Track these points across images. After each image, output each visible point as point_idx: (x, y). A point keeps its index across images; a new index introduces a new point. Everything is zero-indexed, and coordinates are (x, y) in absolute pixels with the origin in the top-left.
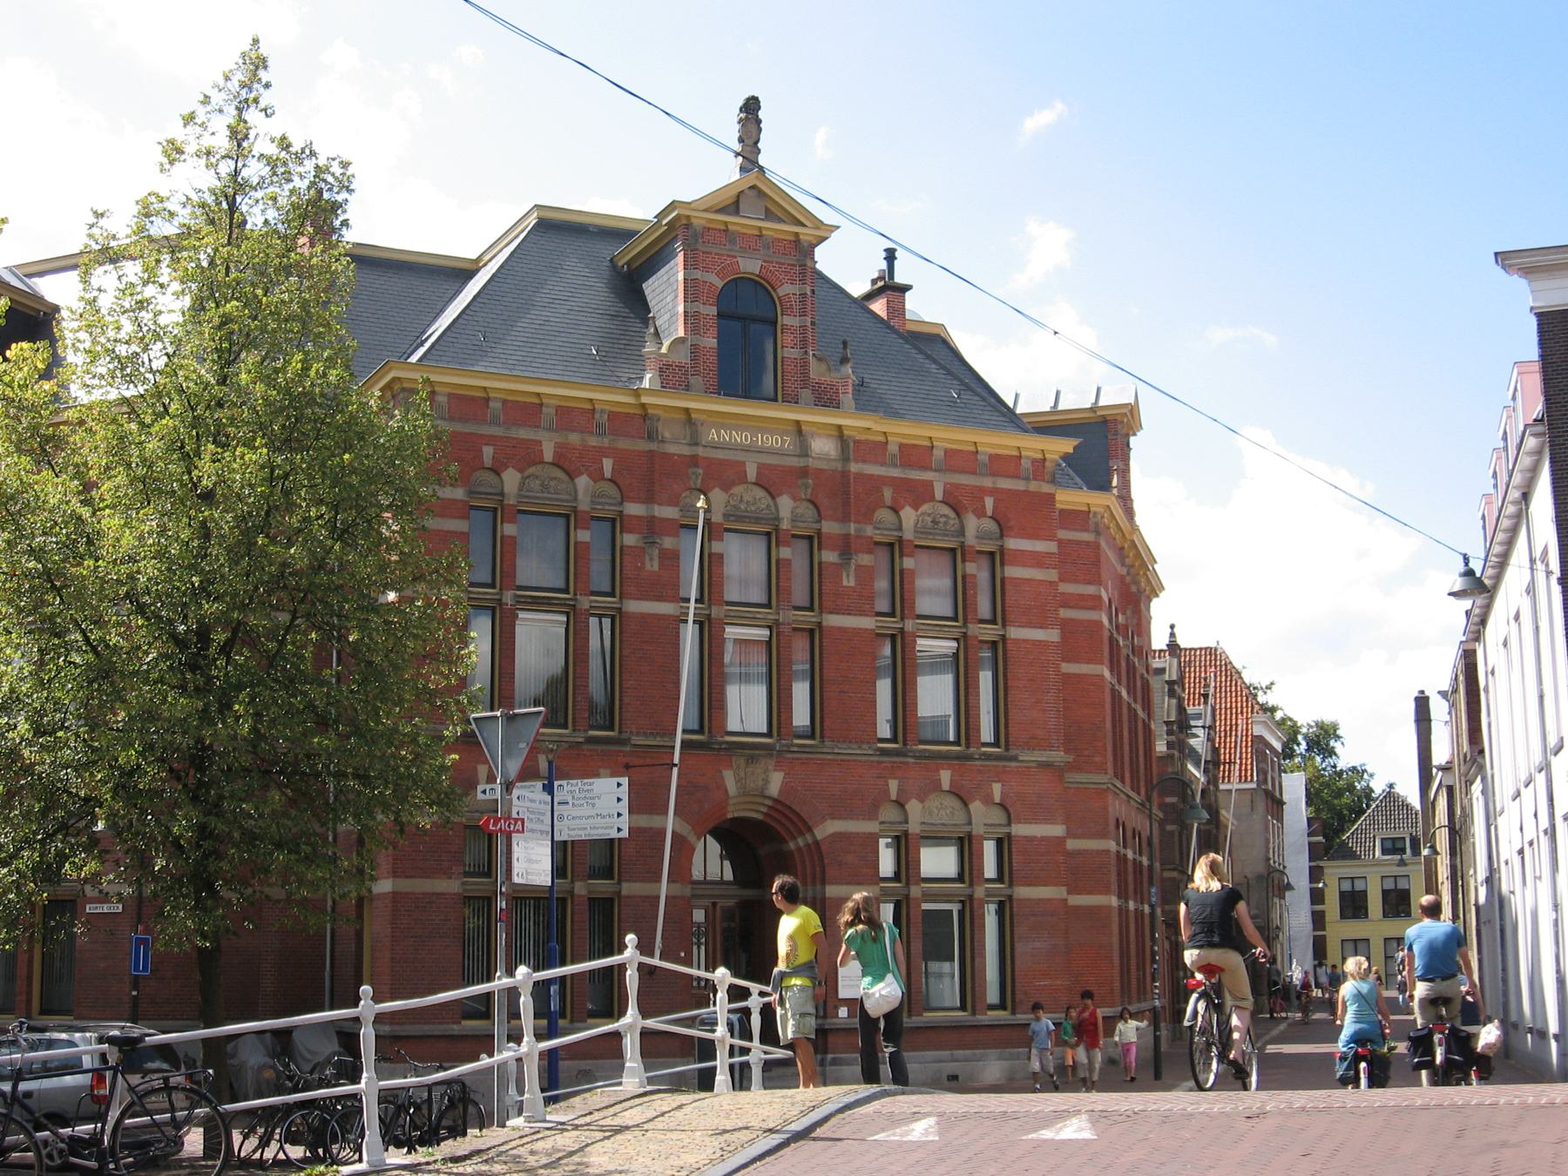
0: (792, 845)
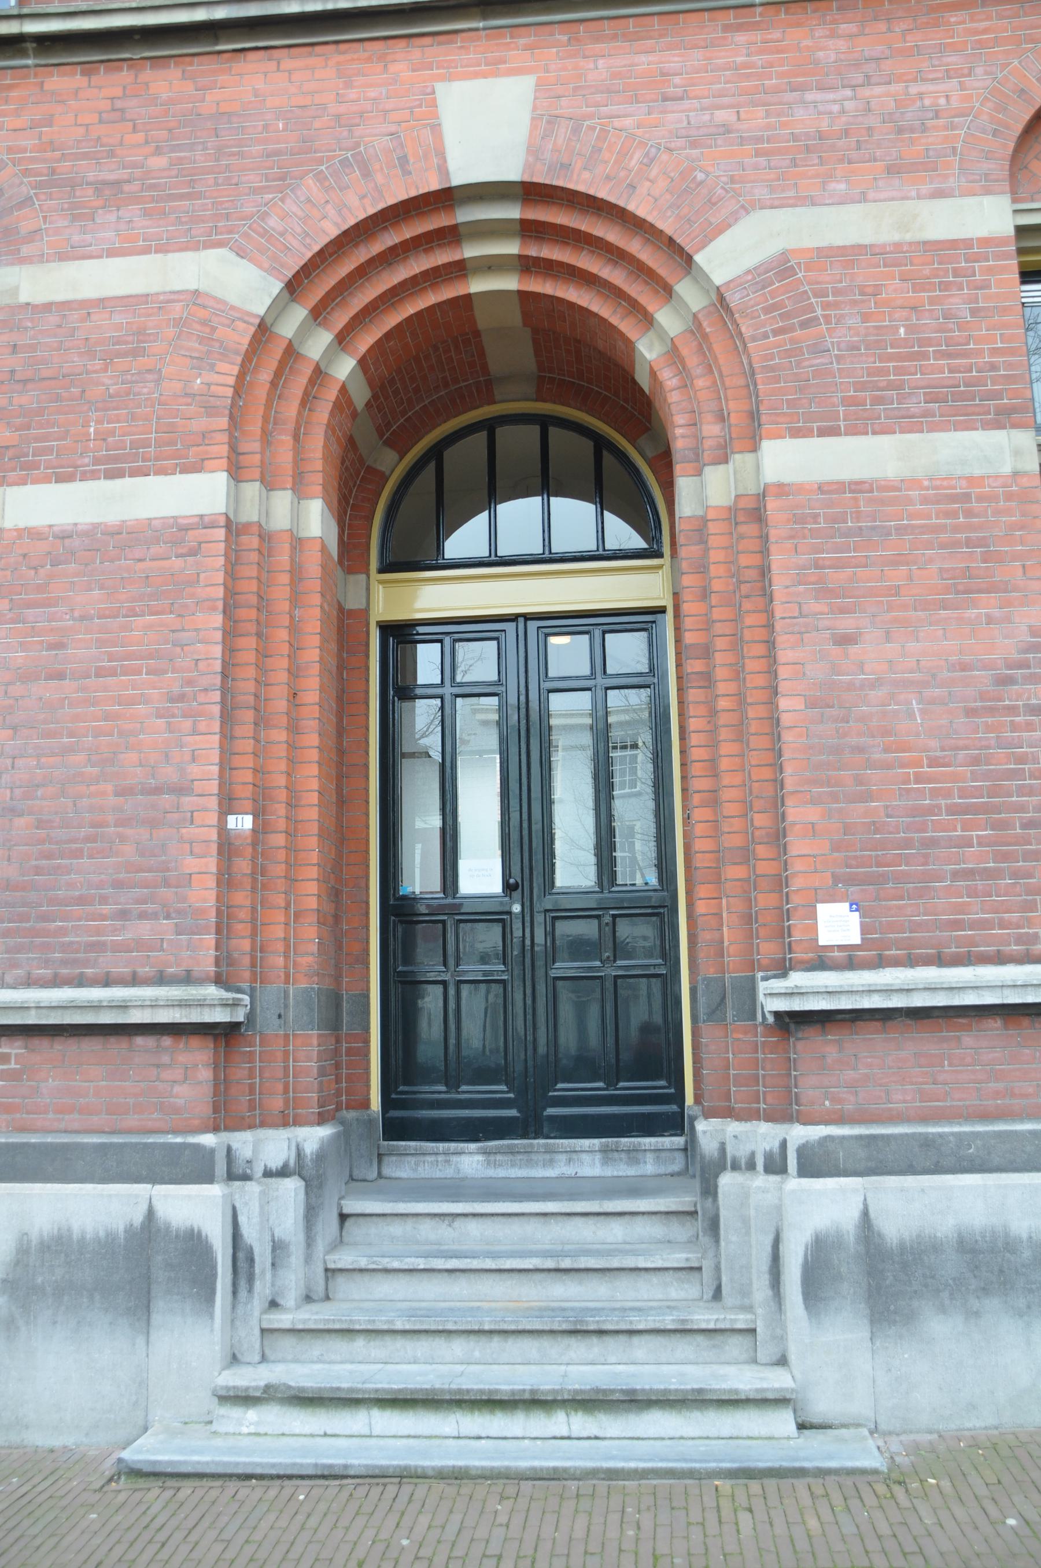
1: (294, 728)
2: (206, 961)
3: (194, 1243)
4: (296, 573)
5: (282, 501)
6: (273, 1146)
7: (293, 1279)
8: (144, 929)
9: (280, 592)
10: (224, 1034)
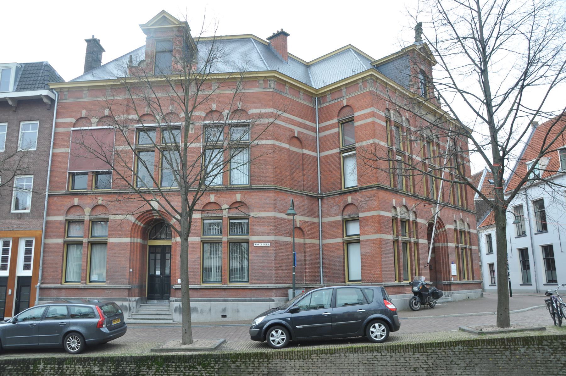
0: (142, 225)
1: (136, 261)
2: (128, 282)
3: (126, 307)
4: (137, 246)
5: (136, 239)
6: (133, 299)
7: (135, 310)
8: (122, 280)
9: (135, 248)
10: (129, 289)
